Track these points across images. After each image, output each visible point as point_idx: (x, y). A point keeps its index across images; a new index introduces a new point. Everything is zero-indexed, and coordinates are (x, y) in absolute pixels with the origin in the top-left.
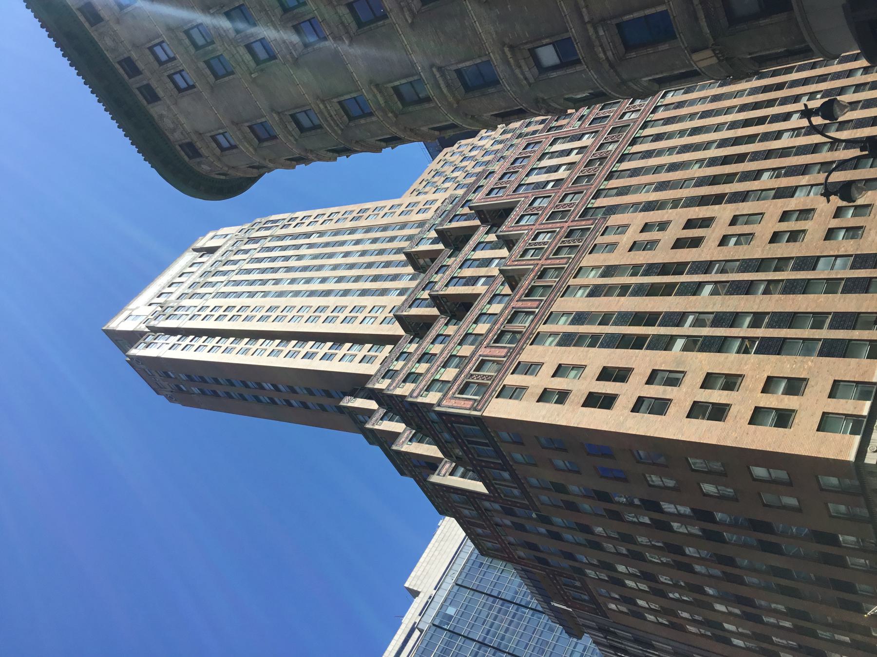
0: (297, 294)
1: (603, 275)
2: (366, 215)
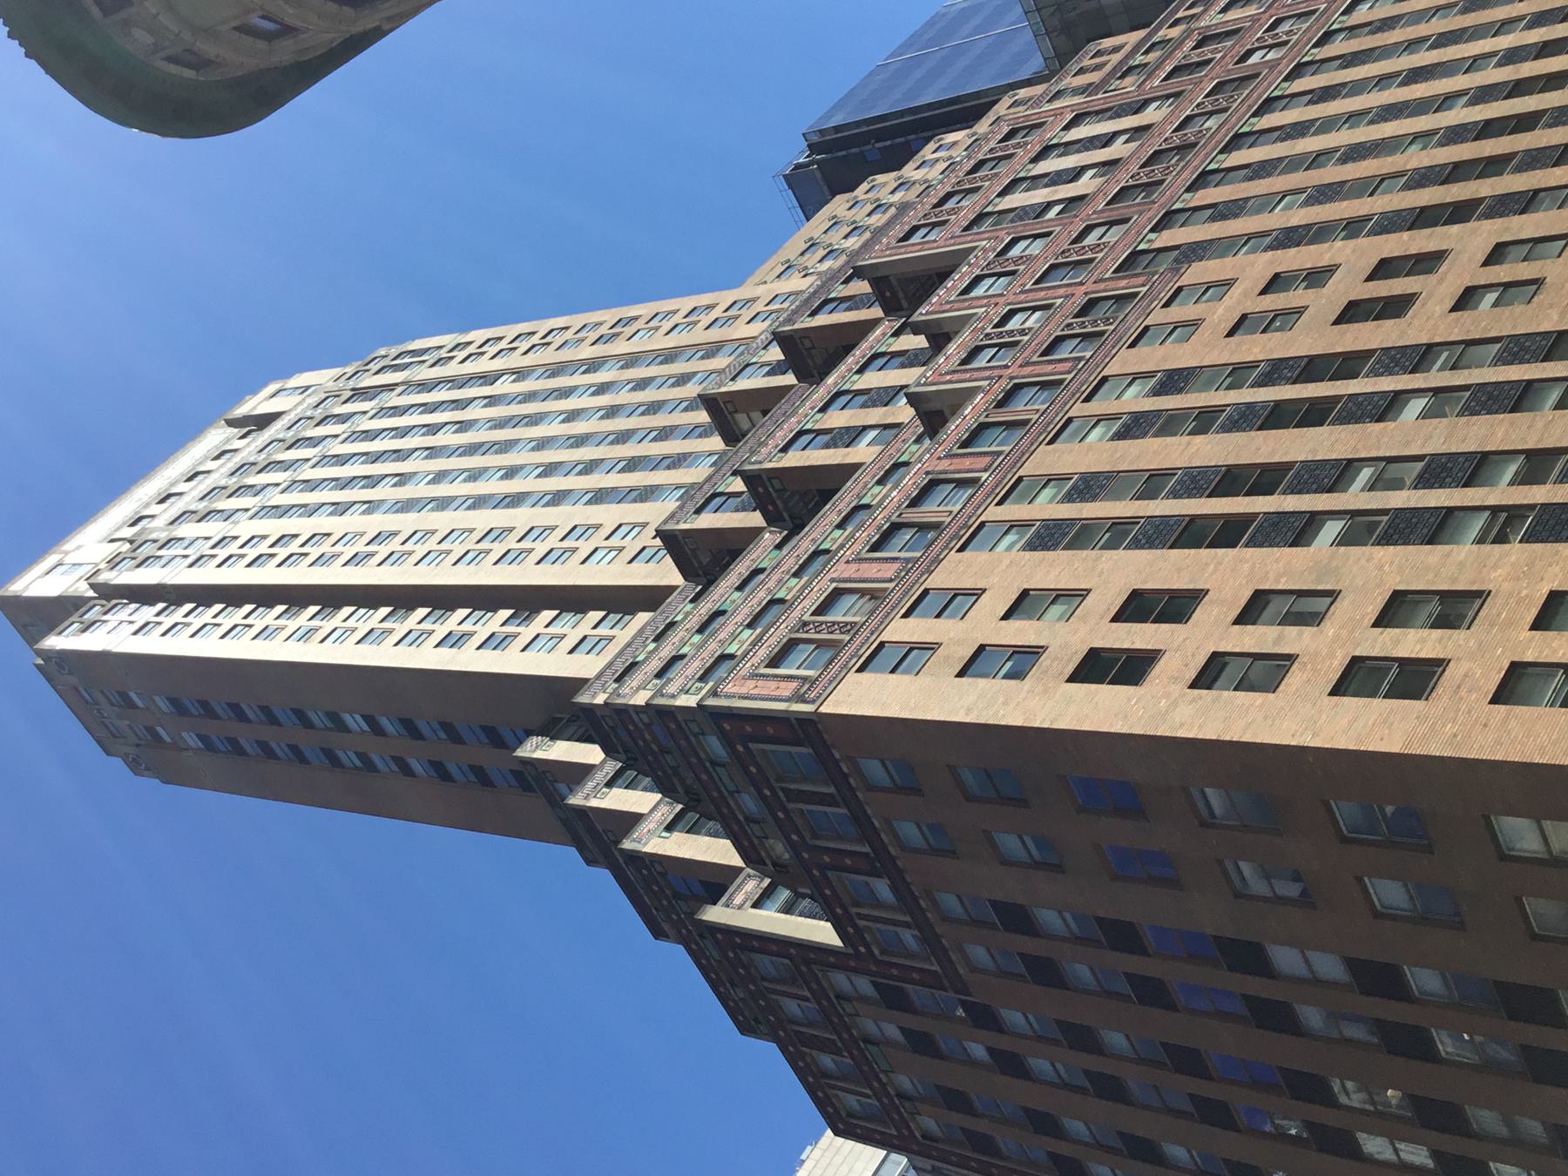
0: (443, 503)
1: (1157, 392)
2: (629, 330)
